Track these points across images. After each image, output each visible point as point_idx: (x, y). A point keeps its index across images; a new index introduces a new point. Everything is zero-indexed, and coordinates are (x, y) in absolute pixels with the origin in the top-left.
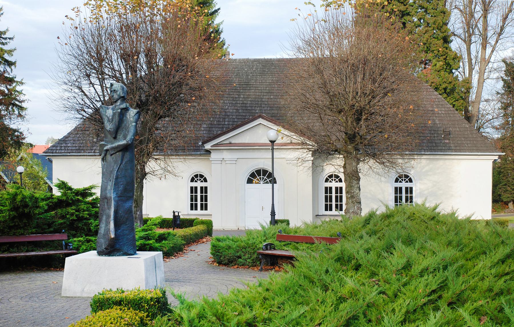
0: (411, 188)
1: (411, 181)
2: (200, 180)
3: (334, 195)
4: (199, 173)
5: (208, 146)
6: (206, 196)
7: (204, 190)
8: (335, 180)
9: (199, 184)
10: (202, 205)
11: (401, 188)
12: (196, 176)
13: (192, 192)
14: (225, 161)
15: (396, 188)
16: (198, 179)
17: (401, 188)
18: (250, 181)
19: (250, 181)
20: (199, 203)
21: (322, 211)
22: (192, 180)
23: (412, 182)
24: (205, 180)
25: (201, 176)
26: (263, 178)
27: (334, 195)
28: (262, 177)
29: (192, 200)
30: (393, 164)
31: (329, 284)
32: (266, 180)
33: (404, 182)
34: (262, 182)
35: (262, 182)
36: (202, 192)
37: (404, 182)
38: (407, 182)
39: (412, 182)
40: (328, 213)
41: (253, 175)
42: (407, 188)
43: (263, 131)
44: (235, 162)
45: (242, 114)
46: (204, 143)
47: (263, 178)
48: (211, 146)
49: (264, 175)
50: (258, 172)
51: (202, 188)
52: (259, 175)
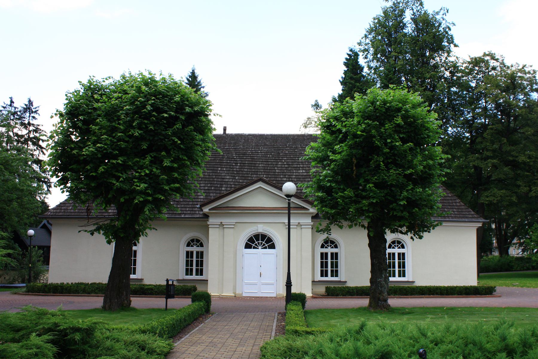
0: (337, 254)
2: (196, 244)
5: (206, 210)
6: (404, 263)
7: (335, 256)
10: (399, 271)
12: (193, 240)
14: (301, 225)
15: (187, 252)
16: (194, 244)
17: (326, 254)
19: (248, 246)
20: (194, 268)
21: (318, 278)
22: (188, 245)
23: (203, 246)
25: (198, 241)
26: (262, 243)
29: (187, 265)
30: (327, 230)
31: (89, 355)
32: (264, 245)
33: (396, 248)
34: (260, 247)
35: (260, 247)
37: (396, 248)
39: (203, 246)
41: (251, 240)
43: (258, 197)
44: (233, 226)
45: (238, 181)
46: (202, 206)
47: (258, 243)
48: (210, 210)
49: (262, 240)
51: (197, 253)
52: (258, 240)
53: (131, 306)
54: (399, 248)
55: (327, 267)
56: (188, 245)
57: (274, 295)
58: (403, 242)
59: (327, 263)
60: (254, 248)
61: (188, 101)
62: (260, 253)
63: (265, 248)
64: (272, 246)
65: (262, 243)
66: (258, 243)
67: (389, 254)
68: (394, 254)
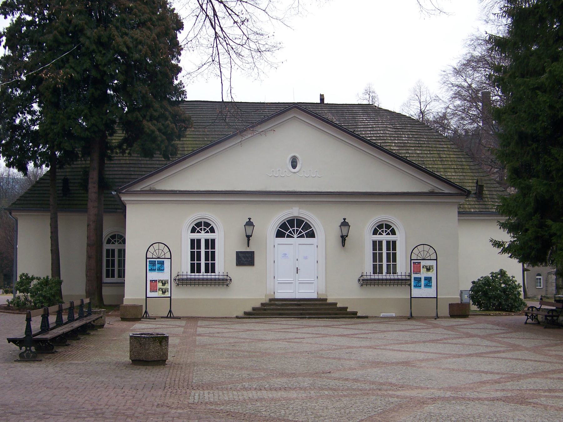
0: (213, 241)
1: (212, 231)
3: (203, 250)
4: (203, 220)
7: (211, 244)
8: (205, 229)
9: (384, 238)
11: (199, 241)
13: (374, 249)
18: (280, 234)
19: (280, 234)
22: (193, 230)
24: (212, 231)
26: (297, 230)
27: (203, 250)
28: (295, 228)
32: (301, 232)
34: (295, 236)
36: (388, 249)
38: (207, 232)
40: (196, 275)
41: (283, 226)
42: (207, 241)
47: (294, 230)
48: (129, 182)
50: (291, 222)
51: (207, 241)
52: (292, 226)
53: (125, 303)
54: (388, 234)
55: (381, 260)
56: (193, 230)
57: (315, 296)
58: (393, 226)
59: (381, 254)
60: (289, 236)
61: (517, 198)
62: (294, 244)
63: (302, 236)
64: (311, 235)
65: (297, 230)
66: (294, 230)
67: (108, 251)
68: (113, 251)
